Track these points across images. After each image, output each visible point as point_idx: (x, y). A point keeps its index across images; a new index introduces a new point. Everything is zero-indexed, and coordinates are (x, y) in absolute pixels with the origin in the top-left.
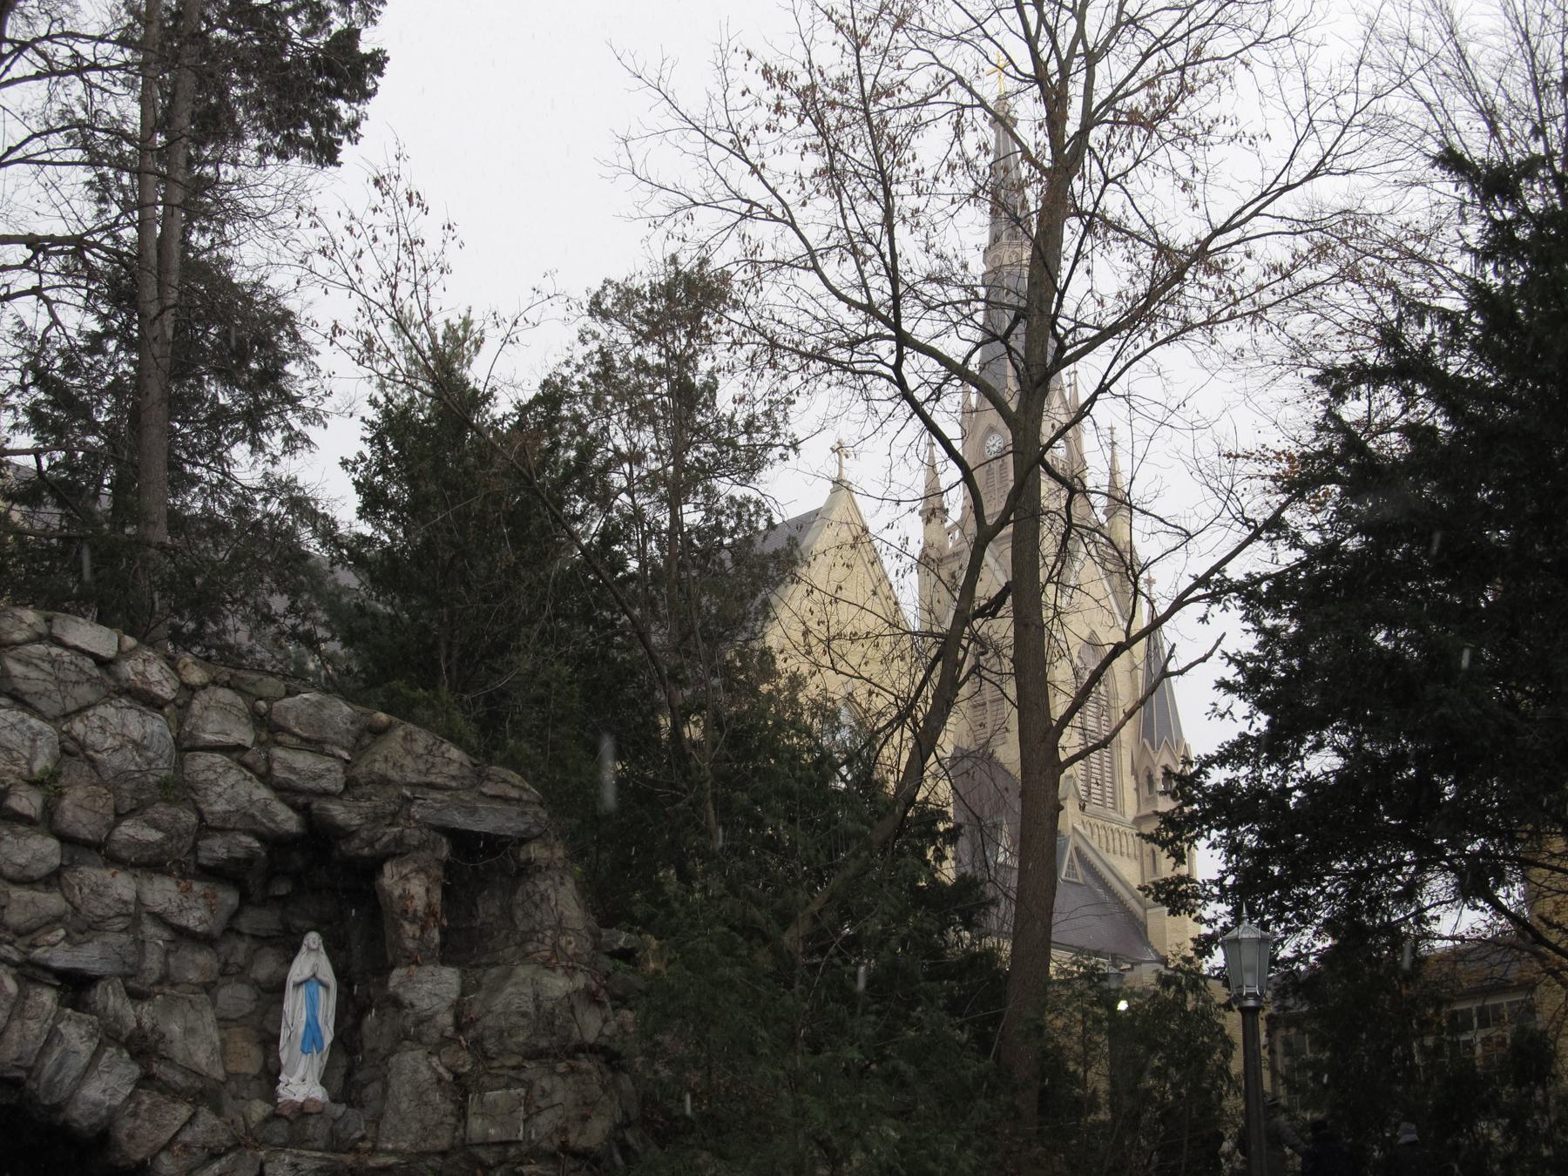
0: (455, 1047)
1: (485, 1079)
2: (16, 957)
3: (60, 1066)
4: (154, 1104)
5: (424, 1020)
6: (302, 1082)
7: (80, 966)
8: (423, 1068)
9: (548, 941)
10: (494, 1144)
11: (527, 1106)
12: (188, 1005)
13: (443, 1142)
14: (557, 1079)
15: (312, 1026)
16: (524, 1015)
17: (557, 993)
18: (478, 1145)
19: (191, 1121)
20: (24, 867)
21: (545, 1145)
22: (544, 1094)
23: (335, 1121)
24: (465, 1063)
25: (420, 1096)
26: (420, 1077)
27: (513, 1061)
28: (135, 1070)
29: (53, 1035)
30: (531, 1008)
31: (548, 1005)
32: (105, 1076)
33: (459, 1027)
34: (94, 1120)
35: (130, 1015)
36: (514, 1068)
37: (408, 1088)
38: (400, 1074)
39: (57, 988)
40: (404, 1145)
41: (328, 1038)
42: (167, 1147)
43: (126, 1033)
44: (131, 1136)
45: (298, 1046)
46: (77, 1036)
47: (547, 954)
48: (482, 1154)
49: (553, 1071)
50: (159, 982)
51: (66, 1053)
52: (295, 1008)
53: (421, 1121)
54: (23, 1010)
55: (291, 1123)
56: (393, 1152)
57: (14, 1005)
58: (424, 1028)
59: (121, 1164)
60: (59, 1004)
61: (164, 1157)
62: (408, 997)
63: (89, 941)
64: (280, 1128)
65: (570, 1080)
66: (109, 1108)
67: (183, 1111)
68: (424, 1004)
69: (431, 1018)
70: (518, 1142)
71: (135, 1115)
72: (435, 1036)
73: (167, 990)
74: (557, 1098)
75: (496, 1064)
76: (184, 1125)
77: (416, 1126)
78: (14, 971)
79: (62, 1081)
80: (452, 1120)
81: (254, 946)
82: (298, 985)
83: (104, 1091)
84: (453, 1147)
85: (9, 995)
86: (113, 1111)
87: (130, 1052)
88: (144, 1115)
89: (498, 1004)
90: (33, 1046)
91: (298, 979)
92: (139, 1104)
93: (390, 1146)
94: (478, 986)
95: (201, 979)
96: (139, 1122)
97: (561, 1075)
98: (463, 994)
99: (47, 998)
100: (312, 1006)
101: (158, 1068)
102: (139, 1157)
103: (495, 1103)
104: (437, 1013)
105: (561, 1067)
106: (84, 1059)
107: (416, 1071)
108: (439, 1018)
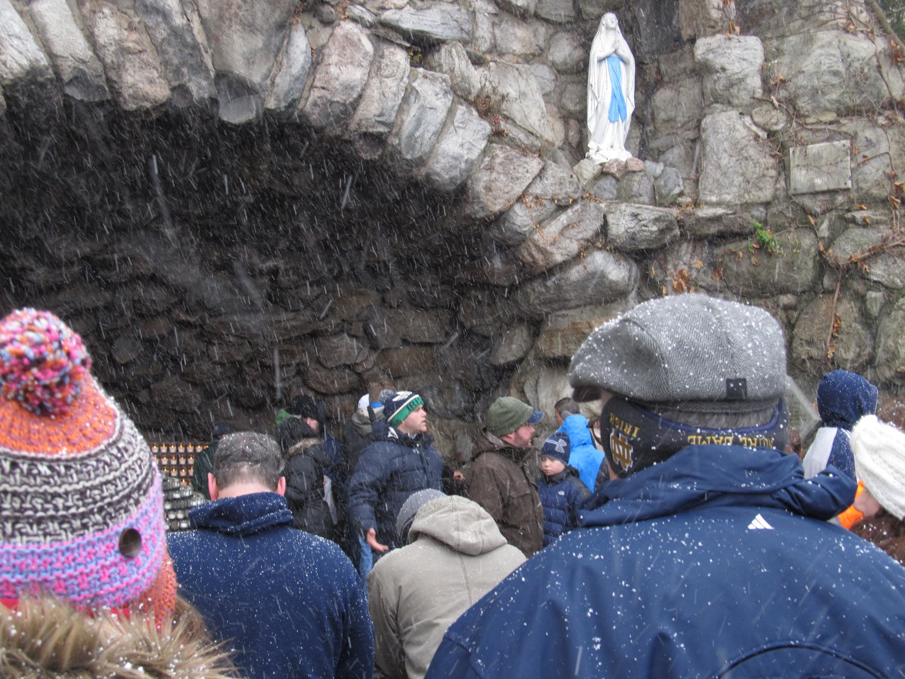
0: (765, 107)
1: (803, 134)
2: (369, 18)
3: (419, 122)
4: (506, 158)
5: (735, 83)
6: (609, 143)
7: (425, 29)
8: (739, 126)
9: (840, 10)
10: (823, 193)
11: (853, 156)
12: (517, 73)
13: (766, 194)
14: (880, 131)
15: (617, 96)
16: (836, 74)
17: (863, 54)
18: (804, 194)
19: (540, 175)
21: (875, 191)
22: (869, 143)
23: (656, 178)
24: (778, 121)
25: (738, 150)
26: (738, 135)
27: (831, 116)
28: (486, 127)
29: (409, 94)
30: (841, 68)
31: (857, 65)
32: (461, 131)
33: (768, 87)
34: (455, 173)
35: (476, 77)
36: (831, 123)
37: (726, 145)
38: (716, 132)
39: (407, 49)
40: (728, 198)
41: (630, 109)
42: (520, 199)
43: (474, 92)
44: (488, 189)
45: (605, 115)
46: (432, 93)
47: (844, 21)
48: (808, 202)
49: (875, 124)
50: (490, 52)
51: (423, 108)
52: (600, 79)
53: (743, 174)
54: (379, 68)
55: (618, 180)
56: (719, 204)
57: (371, 63)
58: (734, 91)
59: (481, 215)
60: (412, 65)
61: (517, 208)
62: (718, 61)
63: (429, 8)
64: (607, 184)
65: (890, 132)
66: (466, 161)
67: (534, 164)
68: (734, 68)
69: (741, 80)
70: (848, 190)
71: (490, 168)
72: (744, 97)
73: (497, 59)
74: (883, 148)
75: (809, 120)
76: (534, 179)
77: (738, 180)
78: (368, 32)
79: (422, 136)
80: (773, 173)
81: (551, 31)
82: (601, 61)
83: (462, 145)
84: (775, 197)
85: (366, 53)
86: (471, 163)
87: (478, 110)
88: (498, 168)
89: (808, 65)
90: (393, 103)
91: (602, 55)
92: (493, 158)
93: (714, 199)
94: (779, 52)
95: (523, 51)
96: (494, 175)
97: (882, 126)
98: (766, 60)
99: (399, 57)
100: (616, 77)
101: (503, 125)
102: (497, 208)
103: (818, 157)
104: (746, 76)
105: (881, 120)
106: (441, 115)
107: (733, 129)
108: (748, 80)
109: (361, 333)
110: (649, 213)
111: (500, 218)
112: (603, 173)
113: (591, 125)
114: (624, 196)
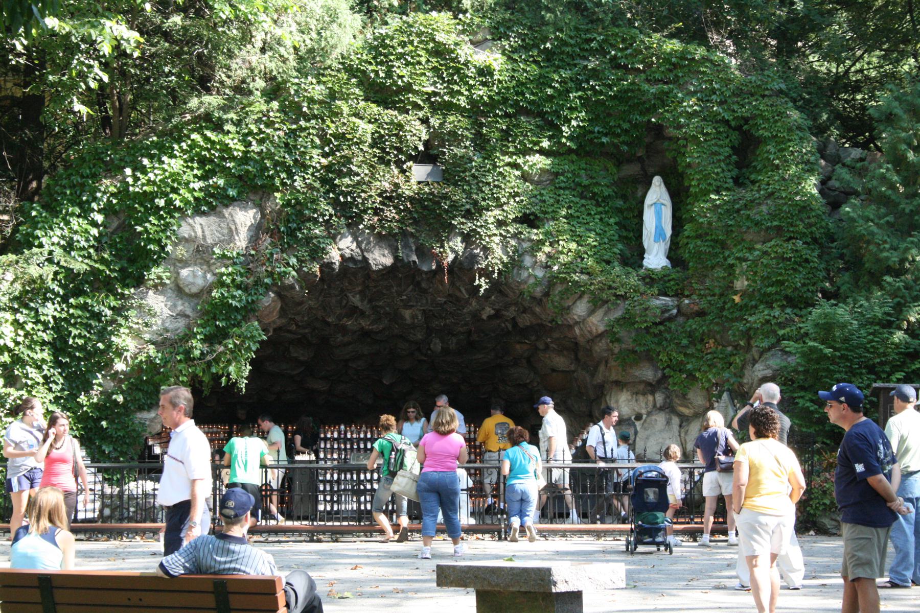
41: (669, 232)
45: (652, 239)
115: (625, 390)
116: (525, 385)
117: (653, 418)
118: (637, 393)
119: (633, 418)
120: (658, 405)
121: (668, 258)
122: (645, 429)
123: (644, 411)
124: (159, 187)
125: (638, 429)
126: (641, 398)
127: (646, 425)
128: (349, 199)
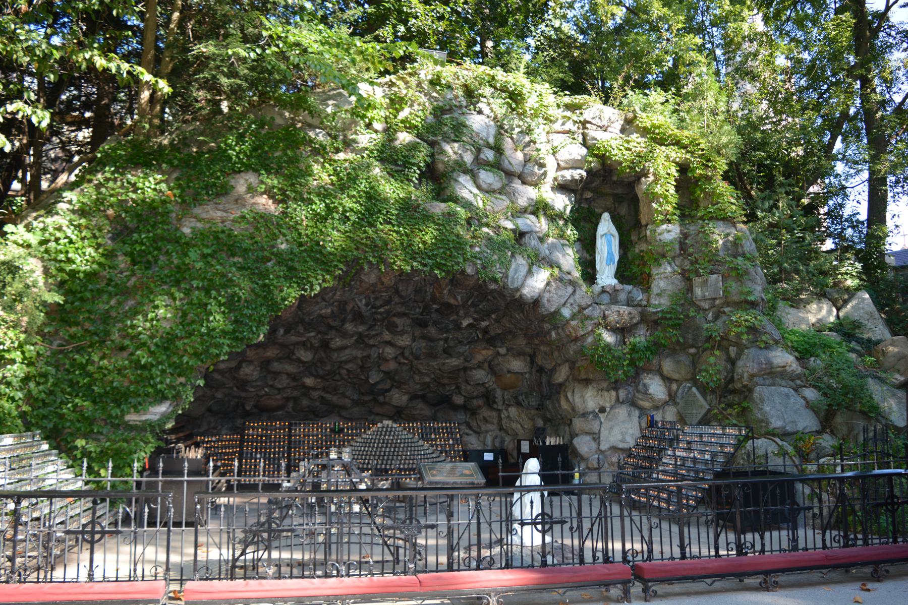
6: (606, 276)
15: (610, 253)
20: (490, 184)
41: (617, 258)
42: (564, 304)
45: (604, 262)
59: (545, 313)
82: (602, 236)
109: (487, 368)
110: (625, 310)
111: (557, 312)
112: (603, 291)
113: (598, 267)
114: (614, 301)
115: (590, 387)
116: (483, 384)
117: (617, 410)
118: (602, 390)
119: (597, 411)
120: (621, 400)
121: (616, 277)
122: (610, 420)
123: (608, 405)
124: (77, 21)
125: (602, 420)
126: (606, 393)
127: (609, 416)
128: (289, 153)
